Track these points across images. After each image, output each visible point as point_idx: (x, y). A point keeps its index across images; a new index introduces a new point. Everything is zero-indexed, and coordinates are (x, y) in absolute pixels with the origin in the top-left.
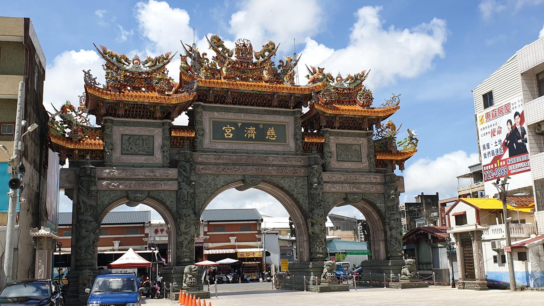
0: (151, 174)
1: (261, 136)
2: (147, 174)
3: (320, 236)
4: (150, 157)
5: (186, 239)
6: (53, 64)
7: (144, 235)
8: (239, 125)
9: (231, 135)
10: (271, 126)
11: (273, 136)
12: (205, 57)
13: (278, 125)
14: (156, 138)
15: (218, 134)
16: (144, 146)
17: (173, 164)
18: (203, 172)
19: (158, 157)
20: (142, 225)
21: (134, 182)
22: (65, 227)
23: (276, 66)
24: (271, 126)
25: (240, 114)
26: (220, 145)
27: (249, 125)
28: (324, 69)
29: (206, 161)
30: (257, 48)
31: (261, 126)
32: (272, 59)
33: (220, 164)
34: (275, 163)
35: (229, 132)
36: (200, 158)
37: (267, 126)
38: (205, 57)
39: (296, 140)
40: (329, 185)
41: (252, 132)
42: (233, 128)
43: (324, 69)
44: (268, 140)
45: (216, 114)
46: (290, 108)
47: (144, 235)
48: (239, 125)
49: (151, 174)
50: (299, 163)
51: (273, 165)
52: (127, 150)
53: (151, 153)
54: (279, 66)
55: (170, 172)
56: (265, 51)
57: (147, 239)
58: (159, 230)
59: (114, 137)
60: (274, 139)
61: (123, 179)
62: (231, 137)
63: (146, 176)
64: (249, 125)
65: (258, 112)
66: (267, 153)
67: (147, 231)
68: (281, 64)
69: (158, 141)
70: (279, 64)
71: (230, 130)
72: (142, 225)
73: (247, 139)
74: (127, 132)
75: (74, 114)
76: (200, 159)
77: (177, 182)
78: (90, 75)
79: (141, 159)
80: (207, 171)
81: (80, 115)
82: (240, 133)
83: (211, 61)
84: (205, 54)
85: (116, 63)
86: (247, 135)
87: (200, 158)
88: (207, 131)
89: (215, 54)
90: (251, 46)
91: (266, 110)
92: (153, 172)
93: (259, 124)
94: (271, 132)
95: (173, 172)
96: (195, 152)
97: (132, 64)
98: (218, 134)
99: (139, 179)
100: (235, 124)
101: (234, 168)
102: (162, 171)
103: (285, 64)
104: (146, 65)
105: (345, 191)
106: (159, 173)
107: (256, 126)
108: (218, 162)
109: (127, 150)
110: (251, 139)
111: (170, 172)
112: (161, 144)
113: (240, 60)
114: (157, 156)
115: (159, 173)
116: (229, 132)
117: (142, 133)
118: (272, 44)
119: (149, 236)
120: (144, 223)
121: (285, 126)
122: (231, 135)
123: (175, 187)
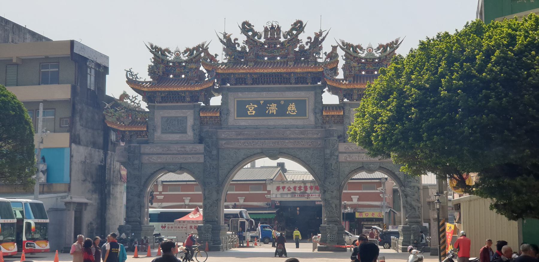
0: (183, 149)
1: (282, 111)
2: (179, 149)
3: (331, 202)
4: (184, 135)
5: (208, 202)
6: (108, 63)
7: (266, 192)
8: (262, 102)
9: (254, 112)
10: (292, 101)
11: (294, 111)
12: (236, 42)
13: (298, 100)
14: (188, 119)
15: (242, 112)
16: (178, 126)
17: (201, 141)
18: (226, 146)
19: (190, 134)
20: (264, 182)
21: (169, 156)
22: (185, 183)
23: (304, 43)
24: (292, 101)
25: (262, 93)
26: (243, 122)
27: (270, 102)
28: (332, 46)
29: (229, 137)
30: (286, 28)
31: (282, 103)
32: (300, 37)
33: (241, 139)
34: (292, 136)
35: (251, 109)
36: (223, 134)
37: (288, 102)
38: (236, 42)
39: (315, 113)
40: (345, 155)
41: (273, 108)
42: (256, 106)
43: (332, 46)
44: (289, 115)
45: (240, 94)
46: (308, 84)
47: (266, 192)
48: (262, 102)
49: (183, 149)
50: (315, 136)
51: (290, 139)
52: (166, 129)
53: (185, 132)
54: (307, 43)
55: (197, 147)
56: (292, 29)
57: (269, 196)
58: (281, 188)
59: (156, 119)
60: (295, 113)
61: (160, 154)
62: (253, 114)
63: (179, 151)
64: (270, 102)
65: (279, 90)
66: (287, 128)
67: (269, 188)
68: (309, 40)
69: (190, 122)
70: (307, 40)
71: (253, 108)
72: (264, 182)
73: (268, 115)
74: (166, 115)
75: (129, 102)
76: (223, 135)
77: (203, 155)
78: (131, 73)
79: (176, 137)
80: (229, 146)
81: (133, 102)
82: (262, 111)
83: (242, 45)
84: (236, 39)
85: (161, 56)
86: (269, 112)
87: (223, 134)
88: (232, 110)
89: (245, 38)
90: (278, 26)
91: (287, 88)
92: (184, 147)
93: (280, 101)
94: (292, 107)
95: (200, 147)
96: (221, 128)
97: (174, 55)
98: (242, 112)
99: (173, 154)
100: (257, 102)
101: (253, 142)
102: (191, 146)
103: (313, 40)
104: (185, 55)
105: (361, 160)
106: (189, 148)
107: (277, 102)
108: (239, 137)
109: (166, 129)
110: (272, 115)
111: (197, 147)
112: (193, 123)
113: (268, 41)
114: (189, 134)
115: (189, 148)
116: (251, 109)
117: (178, 115)
118: (300, 22)
119: (271, 193)
120: (265, 180)
121: (305, 101)
122: (254, 112)
123: (202, 160)
